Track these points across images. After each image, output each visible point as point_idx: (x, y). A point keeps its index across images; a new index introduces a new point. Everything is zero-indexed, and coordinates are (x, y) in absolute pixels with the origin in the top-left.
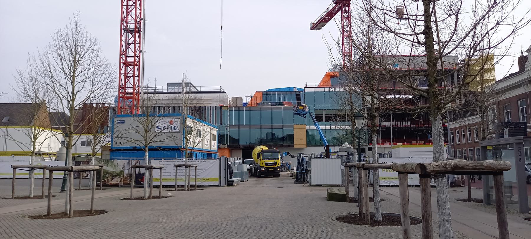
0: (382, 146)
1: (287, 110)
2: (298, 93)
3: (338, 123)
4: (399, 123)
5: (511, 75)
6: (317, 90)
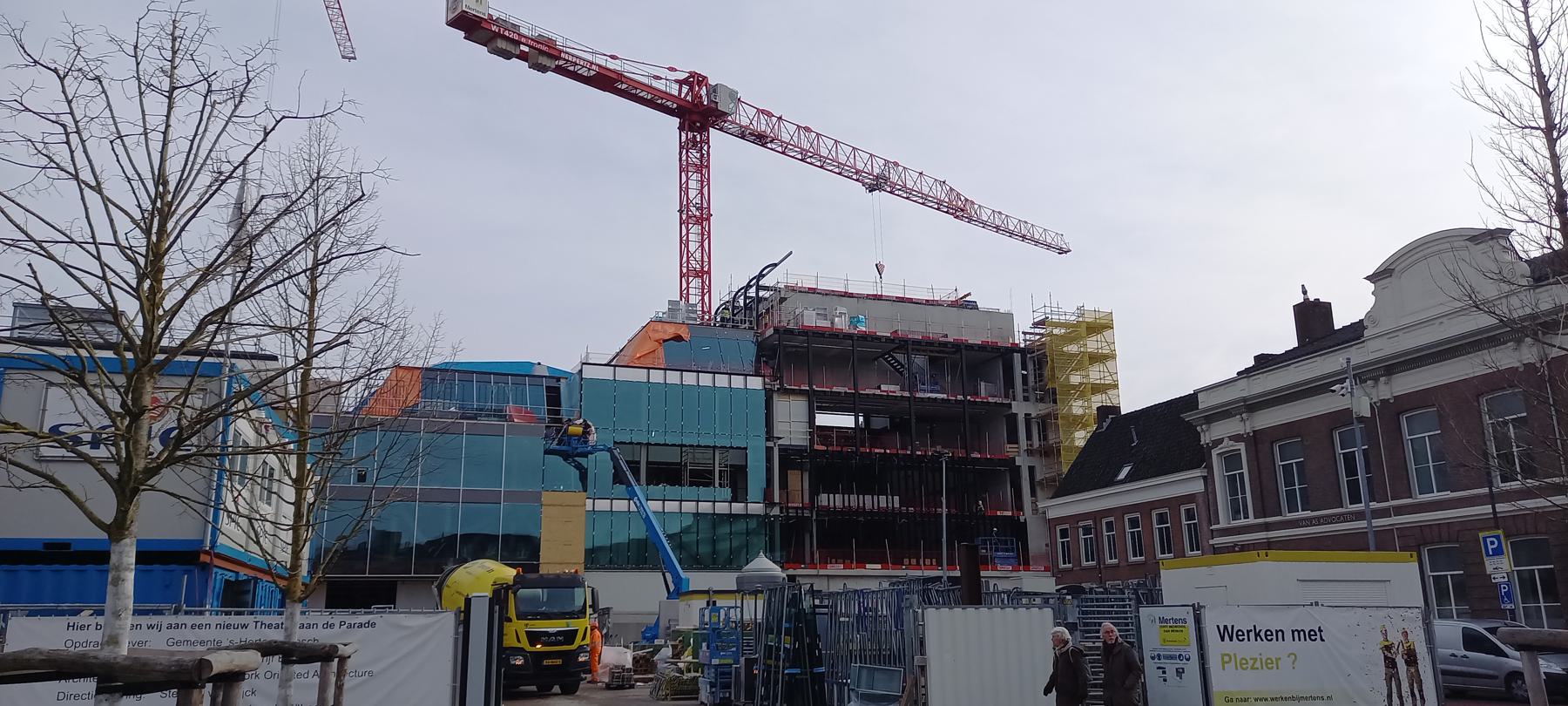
0: (822, 572)
1: (521, 442)
2: (553, 383)
3: (687, 490)
4: (868, 498)
5: (1264, 362)
6: (625, 374)
